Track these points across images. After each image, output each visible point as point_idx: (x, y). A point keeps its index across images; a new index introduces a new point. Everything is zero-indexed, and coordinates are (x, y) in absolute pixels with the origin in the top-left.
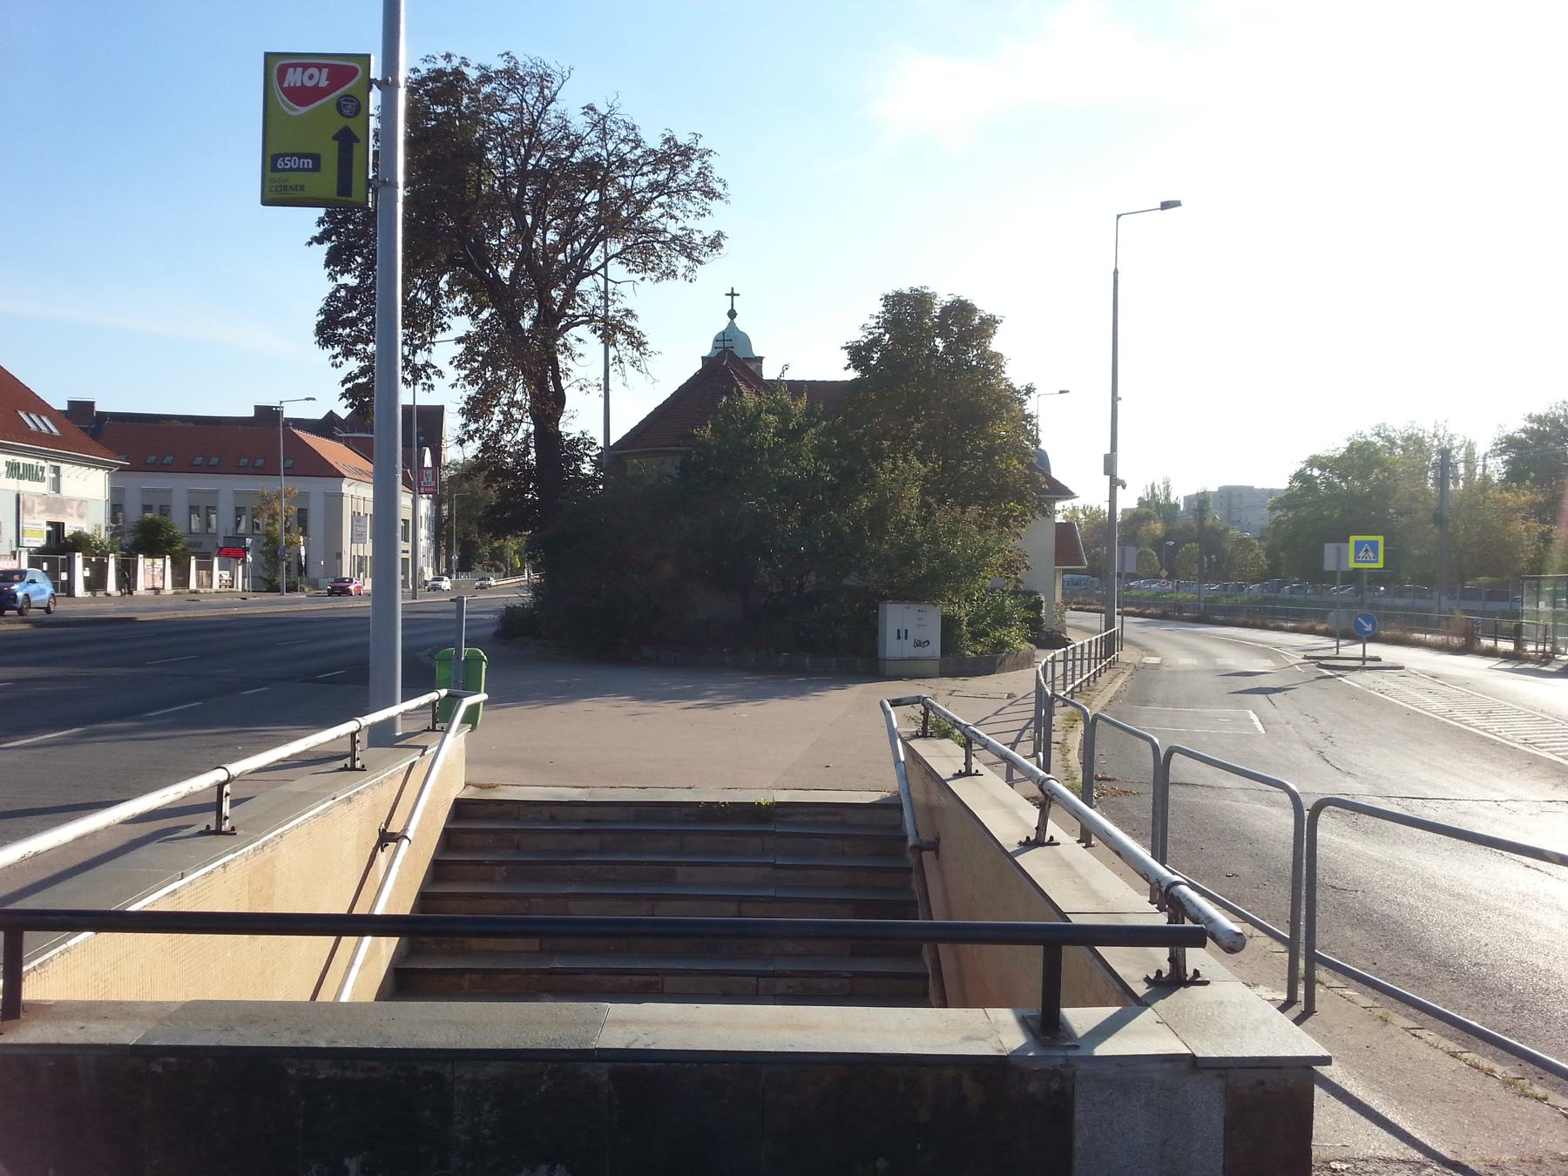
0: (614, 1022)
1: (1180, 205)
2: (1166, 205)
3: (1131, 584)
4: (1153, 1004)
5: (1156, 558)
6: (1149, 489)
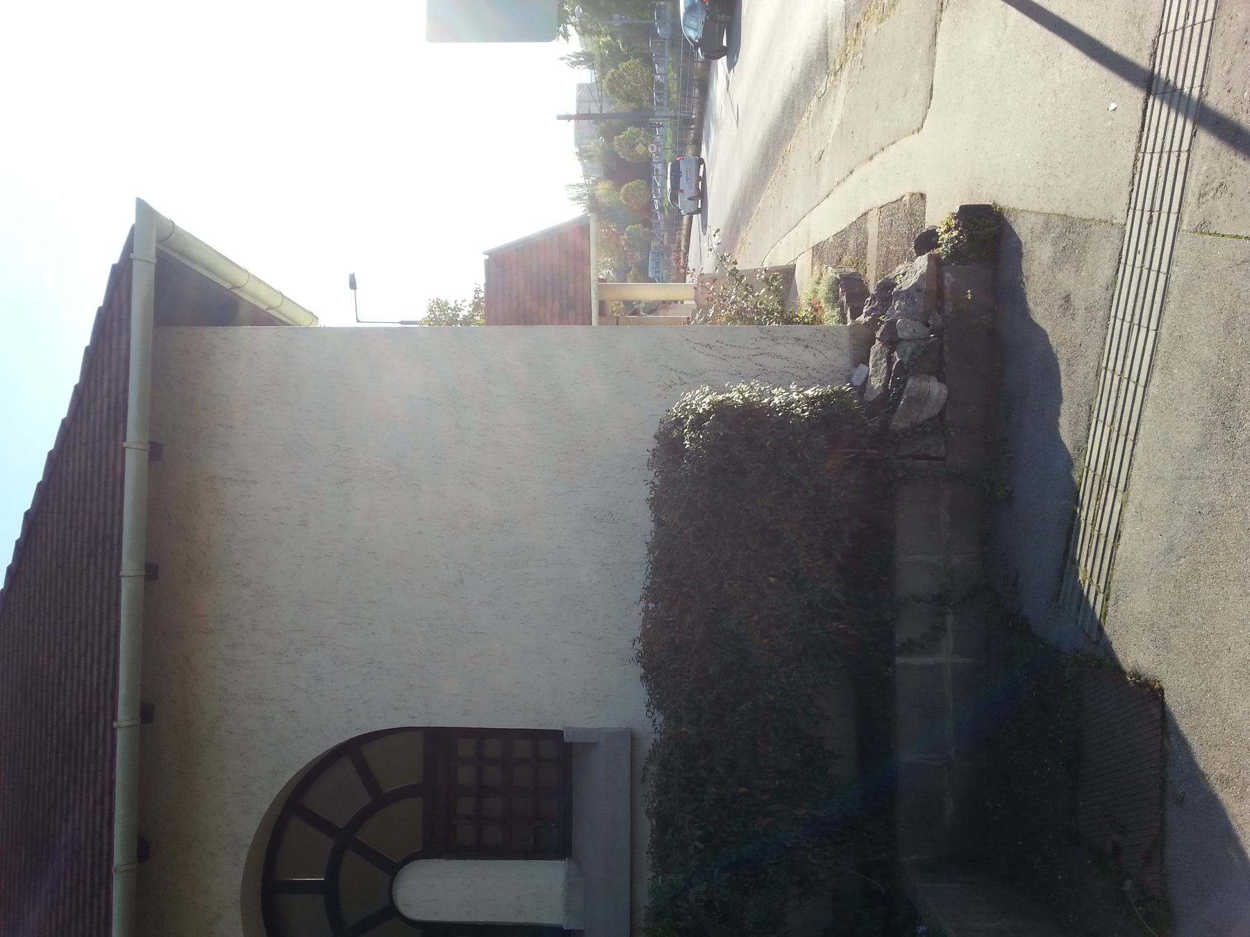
0: (1191, 91)
1: (354, 274)
2: (353, 285)
3: (657, 208)
4: (1143, 70)
5: (630, 184)
6: (575, 202)
